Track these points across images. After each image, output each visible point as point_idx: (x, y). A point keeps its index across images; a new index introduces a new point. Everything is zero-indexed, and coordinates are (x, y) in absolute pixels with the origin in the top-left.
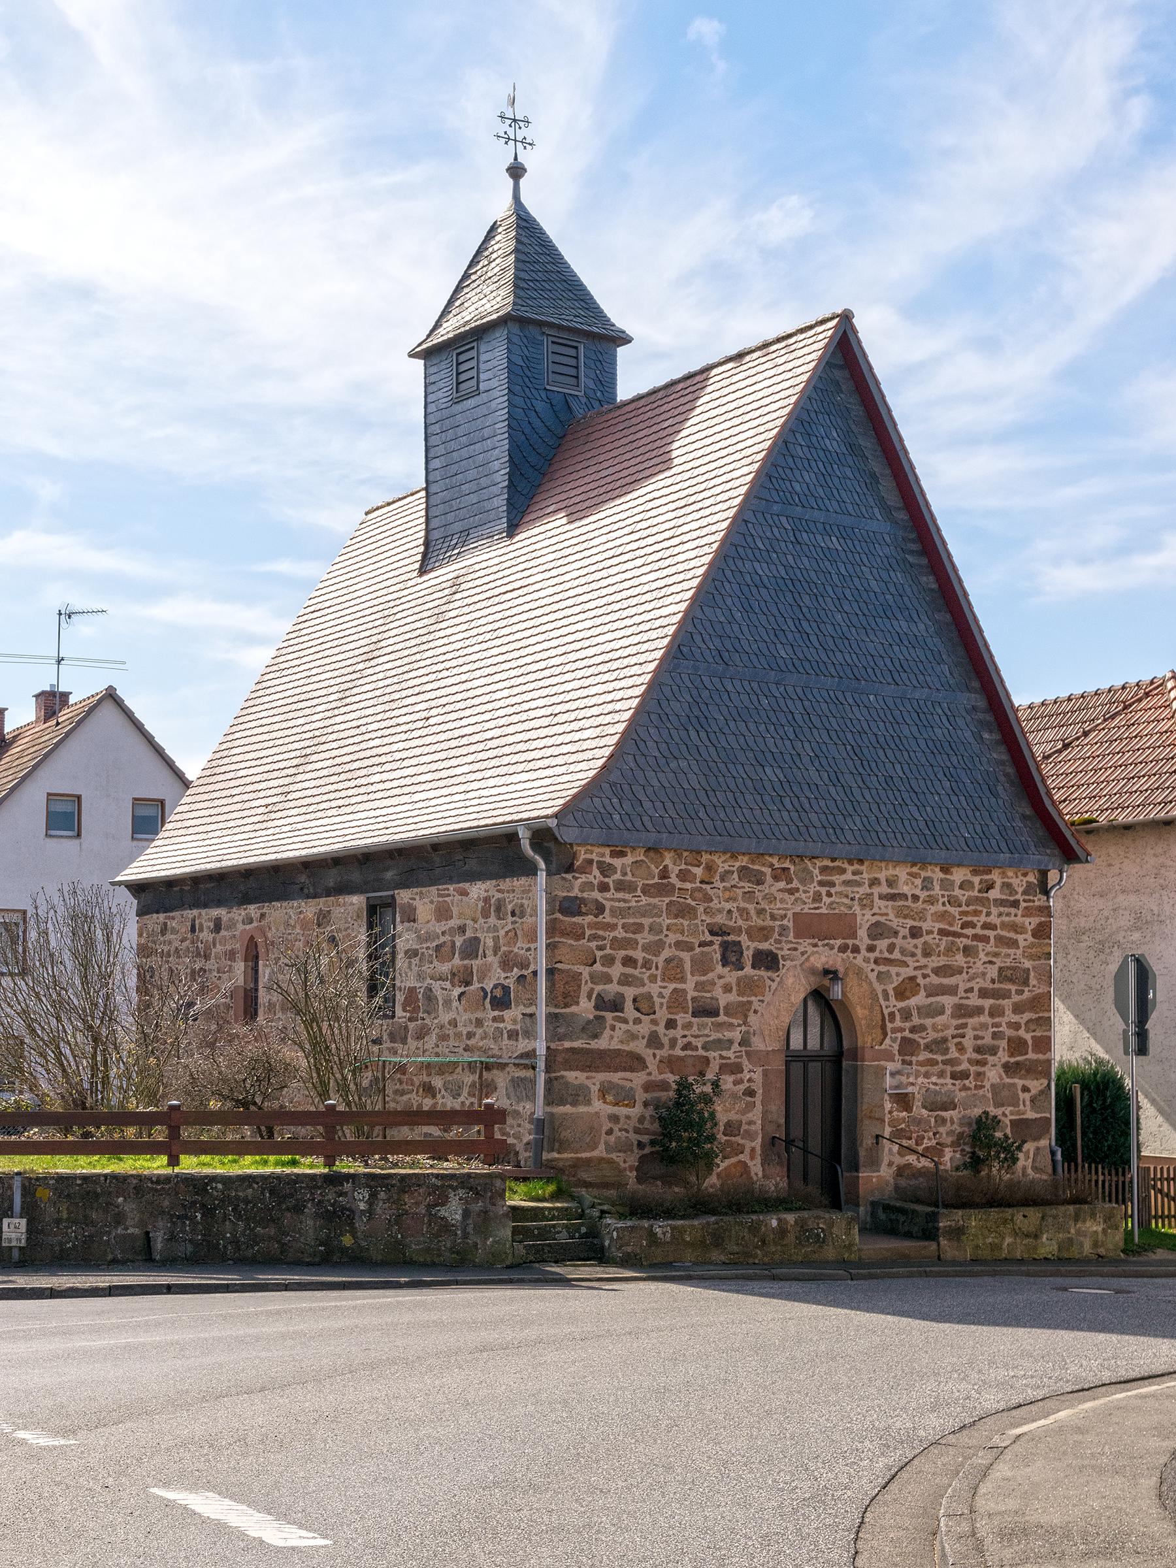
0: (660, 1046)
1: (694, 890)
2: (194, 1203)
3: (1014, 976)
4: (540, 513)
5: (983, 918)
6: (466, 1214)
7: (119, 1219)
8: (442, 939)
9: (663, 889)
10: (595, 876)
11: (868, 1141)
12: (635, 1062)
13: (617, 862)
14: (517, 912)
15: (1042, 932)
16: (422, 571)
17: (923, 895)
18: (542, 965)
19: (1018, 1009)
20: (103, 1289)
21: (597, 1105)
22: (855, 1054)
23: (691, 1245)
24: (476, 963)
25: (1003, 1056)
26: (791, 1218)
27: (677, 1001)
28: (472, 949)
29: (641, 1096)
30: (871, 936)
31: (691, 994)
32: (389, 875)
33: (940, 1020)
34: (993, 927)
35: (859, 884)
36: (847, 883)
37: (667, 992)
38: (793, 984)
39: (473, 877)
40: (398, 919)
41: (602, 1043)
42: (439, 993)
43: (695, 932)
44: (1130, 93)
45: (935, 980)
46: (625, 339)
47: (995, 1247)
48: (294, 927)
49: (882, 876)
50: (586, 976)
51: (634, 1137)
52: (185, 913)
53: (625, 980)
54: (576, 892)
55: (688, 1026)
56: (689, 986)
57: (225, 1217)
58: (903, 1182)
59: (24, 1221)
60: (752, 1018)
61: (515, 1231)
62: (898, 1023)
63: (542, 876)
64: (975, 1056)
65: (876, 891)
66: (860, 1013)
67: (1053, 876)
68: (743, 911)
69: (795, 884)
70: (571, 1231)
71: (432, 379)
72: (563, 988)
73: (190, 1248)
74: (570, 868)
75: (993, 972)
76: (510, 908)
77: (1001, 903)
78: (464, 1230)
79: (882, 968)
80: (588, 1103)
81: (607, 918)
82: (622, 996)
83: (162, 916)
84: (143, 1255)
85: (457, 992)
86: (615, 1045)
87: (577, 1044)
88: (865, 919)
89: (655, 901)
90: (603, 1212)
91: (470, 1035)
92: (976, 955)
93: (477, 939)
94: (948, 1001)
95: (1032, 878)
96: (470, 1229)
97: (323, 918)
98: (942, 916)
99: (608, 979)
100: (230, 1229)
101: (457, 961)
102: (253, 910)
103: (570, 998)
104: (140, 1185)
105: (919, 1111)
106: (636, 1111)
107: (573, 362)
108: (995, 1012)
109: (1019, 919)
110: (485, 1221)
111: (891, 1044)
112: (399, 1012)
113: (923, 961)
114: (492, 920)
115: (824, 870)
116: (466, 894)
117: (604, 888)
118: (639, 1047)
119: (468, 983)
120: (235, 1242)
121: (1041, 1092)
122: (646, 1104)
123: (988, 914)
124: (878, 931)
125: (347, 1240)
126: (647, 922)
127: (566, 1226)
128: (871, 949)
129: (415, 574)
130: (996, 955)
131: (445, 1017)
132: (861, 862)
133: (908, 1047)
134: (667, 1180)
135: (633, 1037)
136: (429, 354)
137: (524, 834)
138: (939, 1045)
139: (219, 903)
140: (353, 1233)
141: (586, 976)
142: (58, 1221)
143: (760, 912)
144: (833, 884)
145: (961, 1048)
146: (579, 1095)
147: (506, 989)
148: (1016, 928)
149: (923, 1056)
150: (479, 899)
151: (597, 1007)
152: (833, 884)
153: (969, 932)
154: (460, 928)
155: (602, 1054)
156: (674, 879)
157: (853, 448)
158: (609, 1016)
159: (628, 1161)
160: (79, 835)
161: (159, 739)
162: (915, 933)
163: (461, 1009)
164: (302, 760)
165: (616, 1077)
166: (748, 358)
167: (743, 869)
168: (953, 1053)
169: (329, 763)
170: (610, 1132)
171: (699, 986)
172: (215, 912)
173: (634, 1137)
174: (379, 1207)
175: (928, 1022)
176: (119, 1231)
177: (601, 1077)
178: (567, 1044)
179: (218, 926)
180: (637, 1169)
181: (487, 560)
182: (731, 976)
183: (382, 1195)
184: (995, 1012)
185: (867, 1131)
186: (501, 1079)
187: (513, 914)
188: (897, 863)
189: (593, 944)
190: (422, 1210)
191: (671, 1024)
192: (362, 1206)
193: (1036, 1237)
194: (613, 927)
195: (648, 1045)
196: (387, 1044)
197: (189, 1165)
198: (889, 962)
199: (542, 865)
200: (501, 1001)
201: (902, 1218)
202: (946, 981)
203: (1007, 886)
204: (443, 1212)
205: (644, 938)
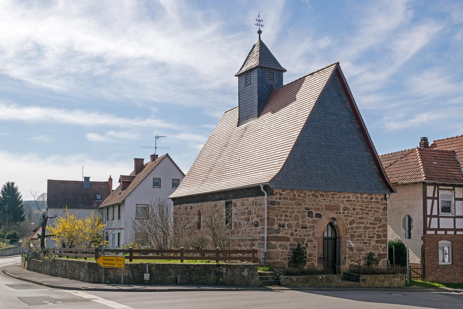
0: (293, 235)
1: (301, 199)
5: (370, 206)
6: (248, 274)
7: (170, 274)
9: (294, 199)
10: (278, 196)
13: (283, 193)
15: (385, 209)
16: (238, 126)
17: (356, 200)
21: (279, 249)
22: (340, 238)
24: (251, 216)
25: (375, 239)
26: (324, 276)
28: (249, 213)
29: (289, 247)
31: (301, 223)
33: (360, 230)
34: (373, 208)
35: (341, 198)
36: (338, 197)
37: (295, 223)
38: (325, 221)
41: (280, 235)
42: (242, 223)
49: (346, 196)
51: (287, 257)
53: (285, 220)
54: (274, 200)
55: (300, 231)
56: (300, 222)
60: (315, 229)
61: (260, 278)
62: (350, 231)
63: (266, 196)
65: (345, 199)
66: (341, 228)
67: (388, 196)
69: (325, 198)
72: (271, 222)
74: (272, 194)
75: (373, 219)
77: (375, 202)
79: (346, 218)
80: (277, 249)
81: (281, 206)
84: (175, 282)
85: (246, 223)
87: (274, 235)
88: (342, 206)
91: (249, 233)
92: (369, 214)
94: (362, 225)
95: (382, 196)
96: (249, 277)
98: (361, 205)
101: (246, 216)
104: (175, 266)
106: (288, 250)
107: (273, 76)
109: (379, 206)
111: (348, 236)
112: (233, 227)
113: (356, 216)
114: (254, 206)
115: (332, 194)
117: (280, 199)
118: (288, 236)
121: (385, 247)
122: (290, 249)
123: (372, 205)
125: (221, 280)
126: (290, 206)
128: (343, 213)
130: (374, 215)
131: (243, 229)
132: (341, 192)
133: (352, 236)
134: (295, 267)
135: (287, 233)
136: (239, 75)
138: (360, 236)
139: (192, 203)
140: (223, 278)
143: (317, 204)
144: (334, 198)
145: (365, 237)
146: (274, 247)
147: (257, 222)
148: (378, 208)
151: (279, 226)
152: (334, 198)
155: (280, 237)
156: (297, 197)
158: (281, 228)
160: (160, 187)
162: (354, 209)
165: (283, 243)
167: (313, 194)
168: (363, 238)
170: (282, 255)
171: (303, 222)
172: (191, 205)
174: (229, 272)
175: (357, 230)
178: (272, 235)
181: (253, 123)
182: (310, 219)
186: (256, 243)
189: (278, 212)
191: (296, 230)
192: (225, 272)
194: (282, 208)
196: (230, 235)
199: (266, 193)
200: (256, 225)
201: (351, 277)
202: (361, 221)
203: (376, 198)
204: (243, 273)
205: (290, 210)
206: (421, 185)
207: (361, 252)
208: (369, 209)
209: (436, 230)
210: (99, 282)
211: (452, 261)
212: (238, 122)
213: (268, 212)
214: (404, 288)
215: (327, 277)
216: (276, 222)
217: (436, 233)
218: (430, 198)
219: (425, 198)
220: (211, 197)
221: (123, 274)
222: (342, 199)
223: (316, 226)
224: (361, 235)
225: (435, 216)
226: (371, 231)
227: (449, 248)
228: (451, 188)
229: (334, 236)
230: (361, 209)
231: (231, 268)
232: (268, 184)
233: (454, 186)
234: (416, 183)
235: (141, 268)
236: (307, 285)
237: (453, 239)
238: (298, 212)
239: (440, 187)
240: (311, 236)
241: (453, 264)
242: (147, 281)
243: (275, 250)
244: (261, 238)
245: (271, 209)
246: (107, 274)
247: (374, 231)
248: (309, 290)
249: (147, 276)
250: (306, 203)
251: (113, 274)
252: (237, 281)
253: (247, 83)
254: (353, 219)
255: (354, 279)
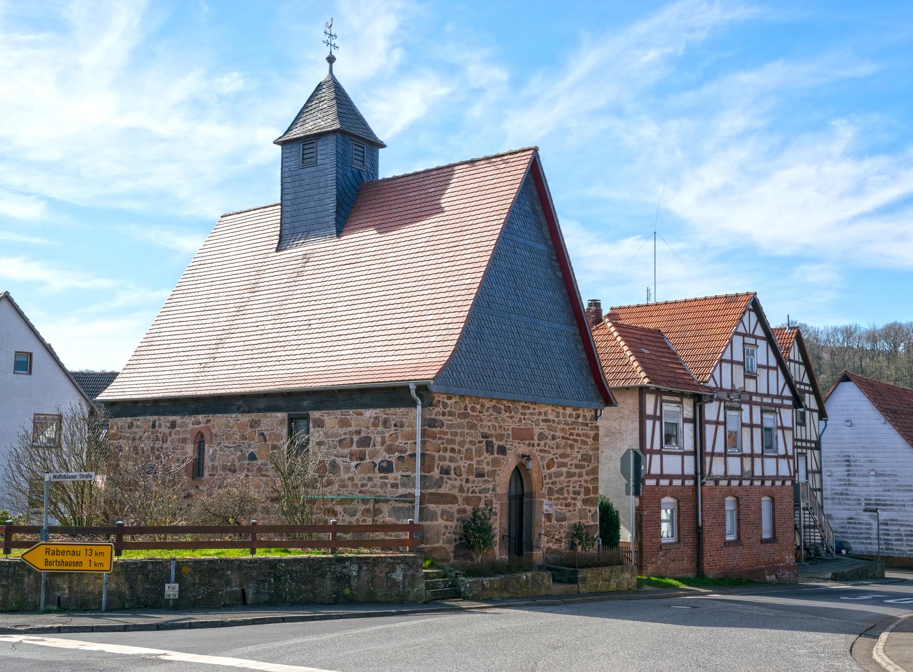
0: (463, 492)
2: (270, 574)
3: (586, 458)
4: (353, 227)
6: (405, 576)
7: (228, 583)
8: (343, 437)
9: (465, 415)
10: (440, 409)
11: (537, 536)
12: (453, 499)
13: (449, 402)
14: (398, 424)
15: (596, 438)
16: (278, 250)
18: (418, 452)
19: (587, 474)
20: (249, 621)
21: (440, 521)
22: (531, 495)
23: (496, 589)
24: (367, 450)
25: (582, 496)
26: (529, 574)
27: (470, 469)
29: (456, 516)
30: (539, 439)
31: (475, 466)
32: (305, 403)
33: (562, 478)
36: (531, 414)
37: (466, 465)
38: (510, 462)
39: (367, 406)
40: (311, 425)
41: (442, 491)
43: (477, 437)
44: (394, 46)
45: (560, 460)
46: (383, 146)
47: (596, 586)
48: (233, 427)
49: (542, 411)
50: (437, 457)
51: (453, 536)
52: (147, 418)
53: (452, 460)
54: (433, 416)
55: (474, 482)
56: (474, 462)
57: (286, 581)
58: (548, 556)
59: (177, 585)
60: (497, 478)
61: (427, 584)
62: (547, 480)
63: (419, 408)
64: (573, 496)
66: (534, 475)
68: (494, 426)
70: (445, 583)
71: (286, 155)
72: (427, 465)
73: (267, 597)
74: (431, 405)
75: (579, 457)
76: (393, 423)
77: (583, 424)
78: (403, 584)
79: (542, 454)
80: (437, 520)
81: (445, 429)
82: (449, 467)
83: (129, 419)
84: (242, 602)
85: (354, 463)
86: (447, 491)
87: (433, 491)
88: (537, 431)
89: (462, 421)
90: (457, 574)
91: (363, 485)
93: (369, 438)
94: (564, 470)
95: (593, 413)
96: (406, 584)
97: (254, 424)
98: (563, 430)
99: (444, 459)
100: (288, 587)
101: (354, 447)
102: (201, 418)
103: (431, 469)
104: (239, 564)
105: (554, 522)
106: (454, 523)
108: (580, 475)
110: (412, 580)
111: (545, 491)
113: (556, 451)
114: (381, 428)
115: (523, 407)
116: (362, 415)
117: (444, 414)
118: (455, 492)
119: (362, 459)
120: (291, 594)
122: (458, 520)
124: (542, 437)
125: (347, 591)
126: (459, 431)
127: (443, 582)
128: (539, 445)
129: (274, 250)
132: (535, 404)
134: (465, 557)
135: (454, 487)
136: (284, 143)
137: (412, 387)
138: (560, 491)
139: (174, 414)
140: (350, 588)
141: (437, 457)
142: (194, 584)
143: (500, 427)
144: (525, 414)
145: (568, 492)
146: (433, 517)
147: (390, 463)
148: (587, 436)
149: (556, 496)
150: (370, 417)
151: (441, 473)
152: (525, 414)
153: (572, 437)
154: (356, 431)
155: (442, 495)
156: (469, 411)
157: (534, 210)
158: (445, 476)
159: (450, 548)
160: (30, 373)
161: (32, 321)
163: (357, 472)
164: (219, 341)
165: (447, 507)
166: (478, 163)
167: (494, 406)
168: (566, 495)
169: (242, 344)
170: (444, 534)
171: (479, 462)
172: (172, 418)
173: (453, 536)
175: (557, 480)
176: (228, 589)
177: (442, 507)
178: (429, 491)
179: (173, 425)
180: (454, 552)
181: (324, 248)
182: (490, 458)
183: (365, 568)
184: (580, 475)
185: (537, 531)
186: (385, 508)
187: (395, 425)
188: (548, 405)
189: (440, 442)
190: (383, 575)
191: (467, 481)
192: (355, 574)
193: (609, 581)
194: (446, 433)
195: (459, 491)
197: (260, 554)
198: (544, 451)
199: (420, 402)
200: (387, 468)
202: (564, 460)
203: (584, 416)
204: (394, 576)
205: (458, 439)
206: (637, 394)
207: (563, 523)
208: (575, 437)
209: (658, 477)
210: (34, 610)
211: (679, 536)
212: (279, 243)
213: (423, 443)
214: (635, 592)
215: (533, 578)
216: (436, 463)
217: (658, 483)
218: (650, 417)
219: (643, 417)
220: (240, 403)
221: (104, 587)
222: (536, 417)
223: (498, 472)
224: (563, 488)
225: (720, 455)
226: (576, 481)
227: (672, 511)
228: (678, 399)
229: (519, 492)
230: (563, 438)
231: (367, 564)
232: (432, 382)
233: (682, 395)
234: (627, 388)
235: (154, 573)
236: (505, 595)
237: (681, 494)
238: (471, 442)
239: (665, 398)
240: (490, 492)
241: (679, 541)
242: (171, 602)
243: (435, 523)
244: (400, 496)
245: (429, 437)
246: (49, 588)
247: (580, 481)
248: (522, 606)
249: (171, 590)
250: (484, 423)
251: (70, 588)
252: (380, 593)
253: (307, 160)
254: (551, 456)
255: (564, 579)
